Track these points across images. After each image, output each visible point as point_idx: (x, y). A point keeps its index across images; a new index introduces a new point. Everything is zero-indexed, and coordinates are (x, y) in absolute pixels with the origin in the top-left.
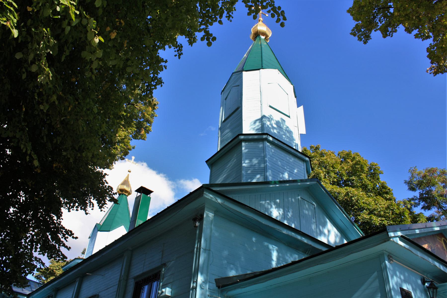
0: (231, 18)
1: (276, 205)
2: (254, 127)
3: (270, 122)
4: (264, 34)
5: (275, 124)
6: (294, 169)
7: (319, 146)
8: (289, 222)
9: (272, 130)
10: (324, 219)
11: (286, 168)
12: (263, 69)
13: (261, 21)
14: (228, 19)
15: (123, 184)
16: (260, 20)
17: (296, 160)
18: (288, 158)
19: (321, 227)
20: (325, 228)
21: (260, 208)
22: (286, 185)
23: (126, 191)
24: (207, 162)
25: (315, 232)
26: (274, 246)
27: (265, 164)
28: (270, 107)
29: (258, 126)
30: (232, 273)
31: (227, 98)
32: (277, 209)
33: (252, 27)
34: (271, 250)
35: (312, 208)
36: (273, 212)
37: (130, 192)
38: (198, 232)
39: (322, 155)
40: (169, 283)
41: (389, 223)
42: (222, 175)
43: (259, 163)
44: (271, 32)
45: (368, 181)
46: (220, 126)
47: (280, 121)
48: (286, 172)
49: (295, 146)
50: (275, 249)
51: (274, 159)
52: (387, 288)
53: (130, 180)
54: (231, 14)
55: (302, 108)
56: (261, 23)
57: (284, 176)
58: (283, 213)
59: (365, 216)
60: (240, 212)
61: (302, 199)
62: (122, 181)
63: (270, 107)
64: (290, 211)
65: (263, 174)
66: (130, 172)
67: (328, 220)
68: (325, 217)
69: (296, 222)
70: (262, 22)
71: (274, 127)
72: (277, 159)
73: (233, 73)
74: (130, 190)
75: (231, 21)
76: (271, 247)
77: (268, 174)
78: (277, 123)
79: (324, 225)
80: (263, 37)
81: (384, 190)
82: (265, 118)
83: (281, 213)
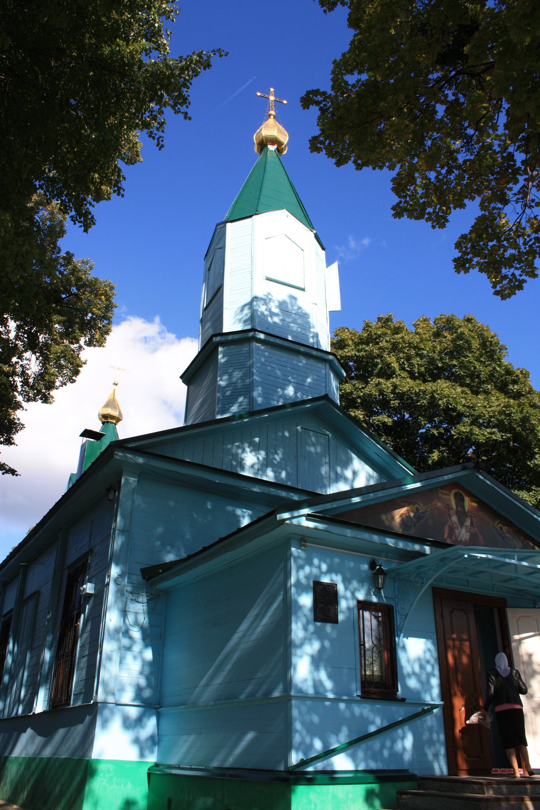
0: (121, 191)
1: (253, 447)
2: (240, 317)
3: (267, 305)
4: (274, 141)
5: (276, 307)
6: (307, 378)
7: (390, 316)
8: (275, 469)
9: (270, 319)
10: (347, 455)
11: (290, 378)
12: (258, 214)
13: (272, 117)
14: (118, 194)
15: (107, 406)
16: (270, 115)
17: (312, 362)
18: (295, 362)
19: (339, 469)
20: (346, 469)
21: (222, 455)
22: (262, 416)
23: (113, 417)
24: (181, 377)
25: (326, 478)
26: (244, 510)
27: (251, 379)
28: (268, 279)
29: (246, 315)
30: (170, 558)
31: (210, 267)
32: (253, 453)
33: (255, 132)
34: (239, 516)
35: (323, 442)
36: (246, 459)
37: (118, 418)
38: (115, 506)
39: (397, 330)
40: (94, 576)
41: (504, 437)
42: (198, 399)
43: (242, 378)
44: (287, 135)
45: (479, 366)
46: (201, 316)
47: (288, 301)
48: (291, 385)
49: (313, 337)
50: (246, 514)
51: (269, 368)
52: (289, 585)
53: (117, 397)
54: (119, 185)
55: (335, 266)
56: (271, 120)
57: (286, 392)
58: (265, 457)
59: (463, 429)
60: (176, 472)
61: (304, 430)
62: (104, 402)
63: (268, 279)
64: (279, 452)
65: (248, 395)
66: (116, 385)
67: (354, 456)
68: (349, 451)
69: (289, 469)
70: (274, 117)
71: (273, 312)
72: (275, 366)
73: (218, 225)
74: (118, 414)
75: (123, 196)
76: (239, 512)
77: (255, 394)
78: (282, 305)
79: (347, 463)
80: (272, 148)
81: (509, 378)
82: (256, 301)
83: (261, 458)
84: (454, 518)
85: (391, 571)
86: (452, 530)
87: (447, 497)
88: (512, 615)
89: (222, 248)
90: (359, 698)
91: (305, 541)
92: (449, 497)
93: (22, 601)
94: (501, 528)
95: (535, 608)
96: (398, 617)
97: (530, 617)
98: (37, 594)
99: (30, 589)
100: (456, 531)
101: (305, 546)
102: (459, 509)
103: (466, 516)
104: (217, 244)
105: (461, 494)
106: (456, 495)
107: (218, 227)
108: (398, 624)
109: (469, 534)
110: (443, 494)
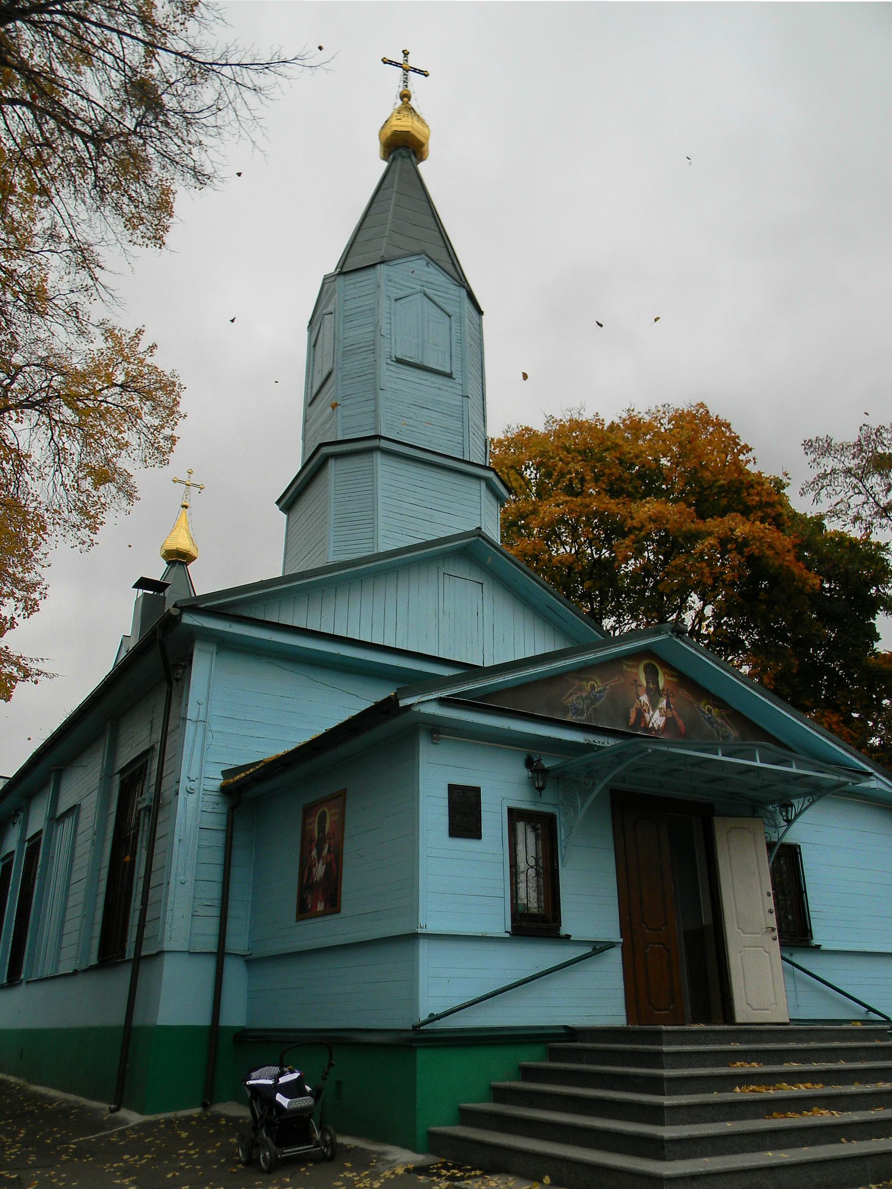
28: (399, 361)
63: (399, 361)
84: (644, 698)
85: (554, 769)
86: (640, 714)
87: (634, 670)
88: (720, 826)
89: (332, 313)
90: (508, 935)
91: (439, 733)
92: (636, 671)
93: (55, 820)
94: (709, 711)
95: (754, 817)
96: (563, 831)
97: (745, 828)
98: (74, 810)
99: (64, 805)
100: (646, 715)
101: (439, 739)
102: (651, 686)
103: (661, 696)
104: (325, 308)
105: (654, 666)
106: (646, 667)
107: (326, 281)
108: (563, 839)
109: (664, 718)
110: (628, 666)
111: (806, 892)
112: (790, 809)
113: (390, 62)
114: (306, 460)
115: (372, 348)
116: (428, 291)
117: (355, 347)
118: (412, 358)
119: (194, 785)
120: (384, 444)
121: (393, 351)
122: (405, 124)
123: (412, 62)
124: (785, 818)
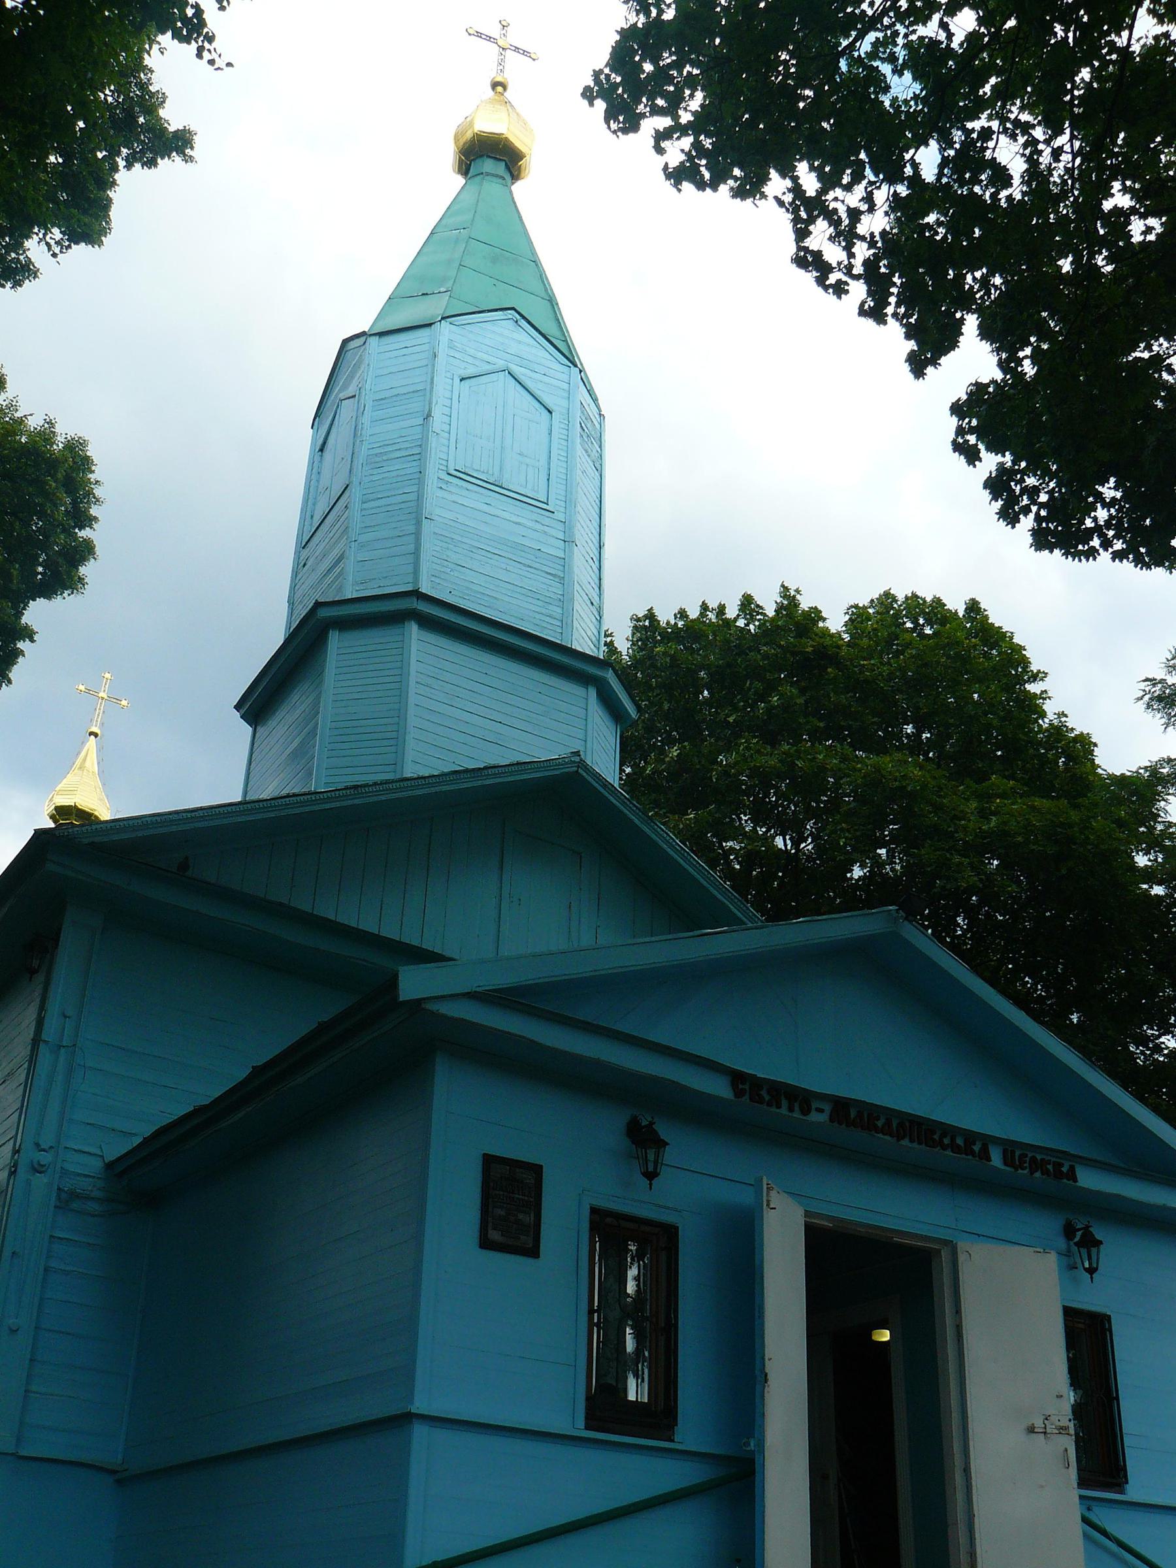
89: (354, 396)
111: (1117, 1398)
112: (1094, 1250)
113: (479, 35)
114: (294, 626)
115: (420, 454)
116: (516, 370)
117: (390, 448)
118: (969, 1372)
119: (45, 1158)
120: (422, 607)
121: (451, 458)
122: (491, 123)
123: (514, 37)
124: (1087, 1265)
